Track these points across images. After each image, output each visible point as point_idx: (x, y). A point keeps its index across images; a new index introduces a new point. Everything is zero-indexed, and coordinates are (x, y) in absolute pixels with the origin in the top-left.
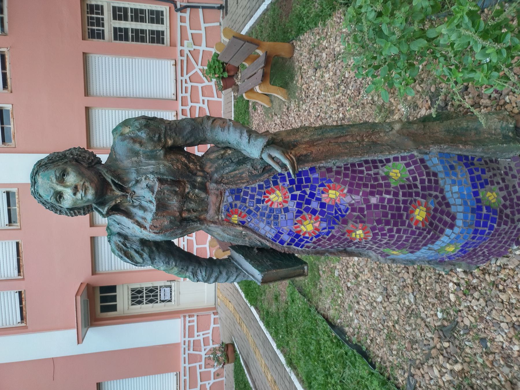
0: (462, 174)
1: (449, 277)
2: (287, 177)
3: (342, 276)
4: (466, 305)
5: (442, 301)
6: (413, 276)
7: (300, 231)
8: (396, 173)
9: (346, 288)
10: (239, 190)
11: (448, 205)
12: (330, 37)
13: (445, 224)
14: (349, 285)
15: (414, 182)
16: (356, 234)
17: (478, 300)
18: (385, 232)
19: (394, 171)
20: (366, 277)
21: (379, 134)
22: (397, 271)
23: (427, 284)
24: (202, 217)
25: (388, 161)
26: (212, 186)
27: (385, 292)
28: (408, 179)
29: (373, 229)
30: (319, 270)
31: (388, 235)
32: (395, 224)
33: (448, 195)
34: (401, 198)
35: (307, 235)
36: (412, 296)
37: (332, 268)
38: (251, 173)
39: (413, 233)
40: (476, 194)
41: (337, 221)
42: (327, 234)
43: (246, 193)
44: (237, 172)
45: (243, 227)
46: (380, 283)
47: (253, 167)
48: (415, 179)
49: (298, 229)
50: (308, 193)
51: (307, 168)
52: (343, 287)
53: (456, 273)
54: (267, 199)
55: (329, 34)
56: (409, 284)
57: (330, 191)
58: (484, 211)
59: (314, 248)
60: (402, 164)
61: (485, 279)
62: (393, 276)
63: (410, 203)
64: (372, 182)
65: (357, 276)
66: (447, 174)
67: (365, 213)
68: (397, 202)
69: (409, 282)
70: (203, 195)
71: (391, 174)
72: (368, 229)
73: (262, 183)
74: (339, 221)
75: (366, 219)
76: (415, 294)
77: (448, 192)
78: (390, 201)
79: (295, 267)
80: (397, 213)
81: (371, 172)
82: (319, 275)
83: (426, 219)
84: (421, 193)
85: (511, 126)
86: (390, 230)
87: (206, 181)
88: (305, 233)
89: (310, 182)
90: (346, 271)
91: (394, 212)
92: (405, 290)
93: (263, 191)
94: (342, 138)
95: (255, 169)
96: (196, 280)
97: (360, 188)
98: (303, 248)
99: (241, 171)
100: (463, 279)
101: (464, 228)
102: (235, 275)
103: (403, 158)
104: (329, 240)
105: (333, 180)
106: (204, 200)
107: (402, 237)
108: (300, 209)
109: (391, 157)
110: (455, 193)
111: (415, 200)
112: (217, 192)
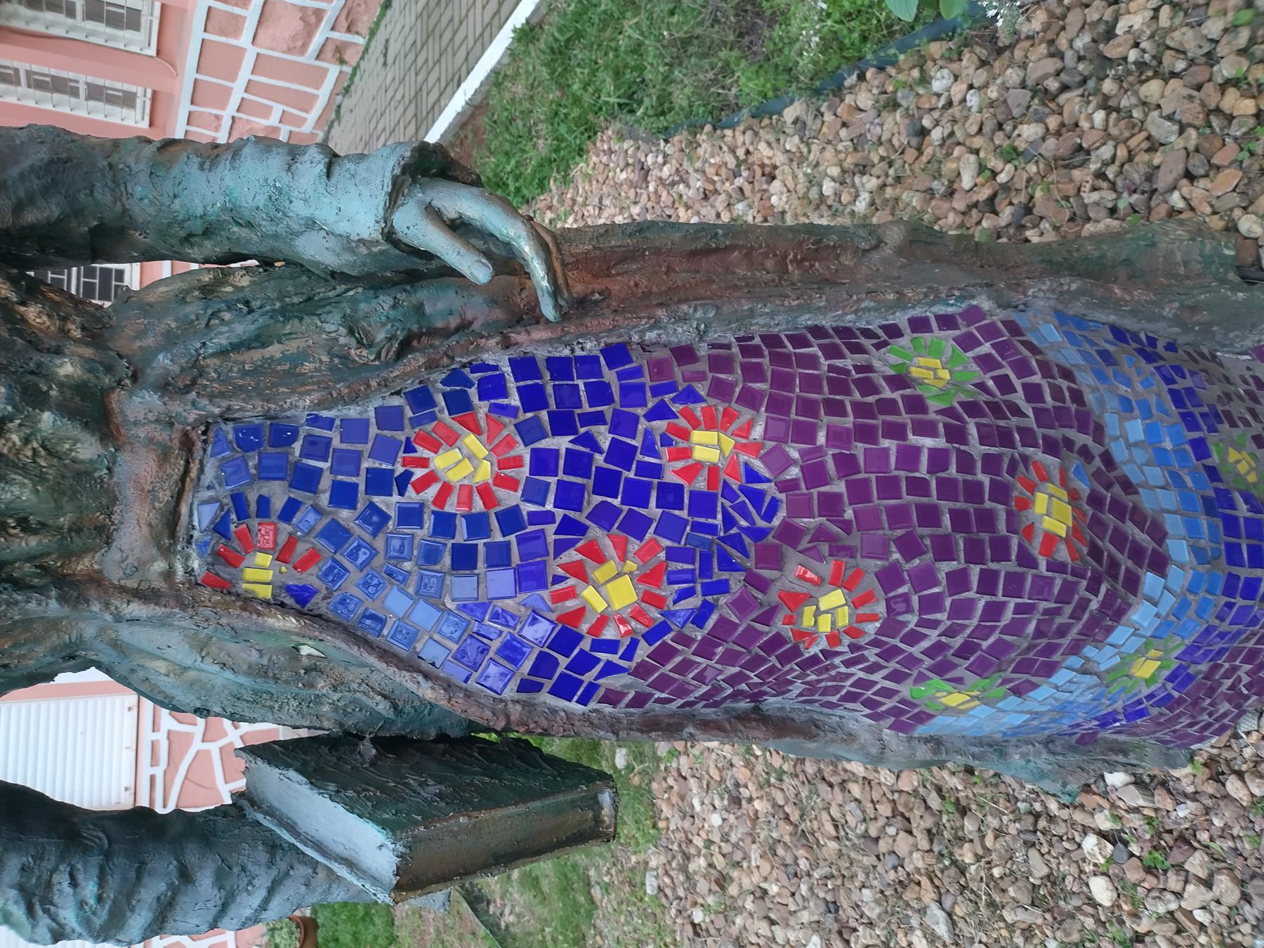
0: (1142, 382)
1: (1079, 816)
2: (510, 378)
3: (668, 891)
4: (1161, 909)
5: (1061, 913)
6: (931, 841)
7: (580, 613)
8: (935, 370)
9: (689, 930)
10: (282, 434)
11: (1128, 486)
12: (585, 205)
13: (1137, 553)
14: (698, 916)
15: (1007, 397)
16: (818, 613)
17: (1208, 884)
18: (936, 590)
19: (922, 361)
20: (756, 878)
21: (837, 257)
22: (866, 836)
23: (994, 856)
24: (83, 565)
25: (893, 332)
26: (137, 407)
27: (829, 921)
28: (981, 386)
29: (890, 578)
30: (589, 885)
31: (948, 602)
32: (974, 555)
33: (1119, 452)
34: (976, 448)
35: (609, 634)
36: (941, 915)
37: (632, 870)
38: (345, 358)
39: (1042, 586)
40: (1200, 448)
41: (736, 556)
42: (699, 618)
43: (317, 447)
44: (274, 350)
45: (300, 614)
46: (811, 889)
47: (351, 332)
48: (1005, 385)
49: (571, 604)
50: (605, 445)
51: (591, 347)
52: (677, 928)
53: (1105, 795)
54: (419, 473)
55: (580, 200)
56: (918, 870)
57: (697, 436)
58: (1243, 510)
59: (640, 700)
60: (946, 339)
61: (1227, 796)
62: (853, 855)
63: (1012, 470)
64: (857, 396)
65: (722, 881)
66: (1100, 376)
67: (849, 514)
68: (966, 463)
69: (920, 864)
70: (88, 449)
71: (915, 372)
72: (870, 582)
73: (397, 401)
74: (747, 556)
75: (854, 540)
76: (947, 903)
77: (1116, 438)
78: (938, 460)
79: (562, 798)
80: (971, 507)
81: (848, 362)
82: (592, 901)
83: (1075, 531)
84: (1040, 432)
85: (1227, 252)
86: (958, 581)
87: (107, 380)
88: (603, 620)
89: (610, 400)
90: (683, 869)
91: (959, 505)
92: (909, 895)
93: (401, 436)
94: (713, 258)
95: (360, 343)
96: (43, 931)
97: (816, 416)
98: (593, 705)
99: (292, 346)
100: (1136, 810)
101: (1200, 568)
102: (263, 881)
103: (947, 322)
104: (705, 649)
105: (702, 389)
106: (88, 474)
107: (1001, 607)
108: (572, 514)
109: (901, 319)
110: (1136, 444)
111: (1025, 459)
112: (162, 435)
